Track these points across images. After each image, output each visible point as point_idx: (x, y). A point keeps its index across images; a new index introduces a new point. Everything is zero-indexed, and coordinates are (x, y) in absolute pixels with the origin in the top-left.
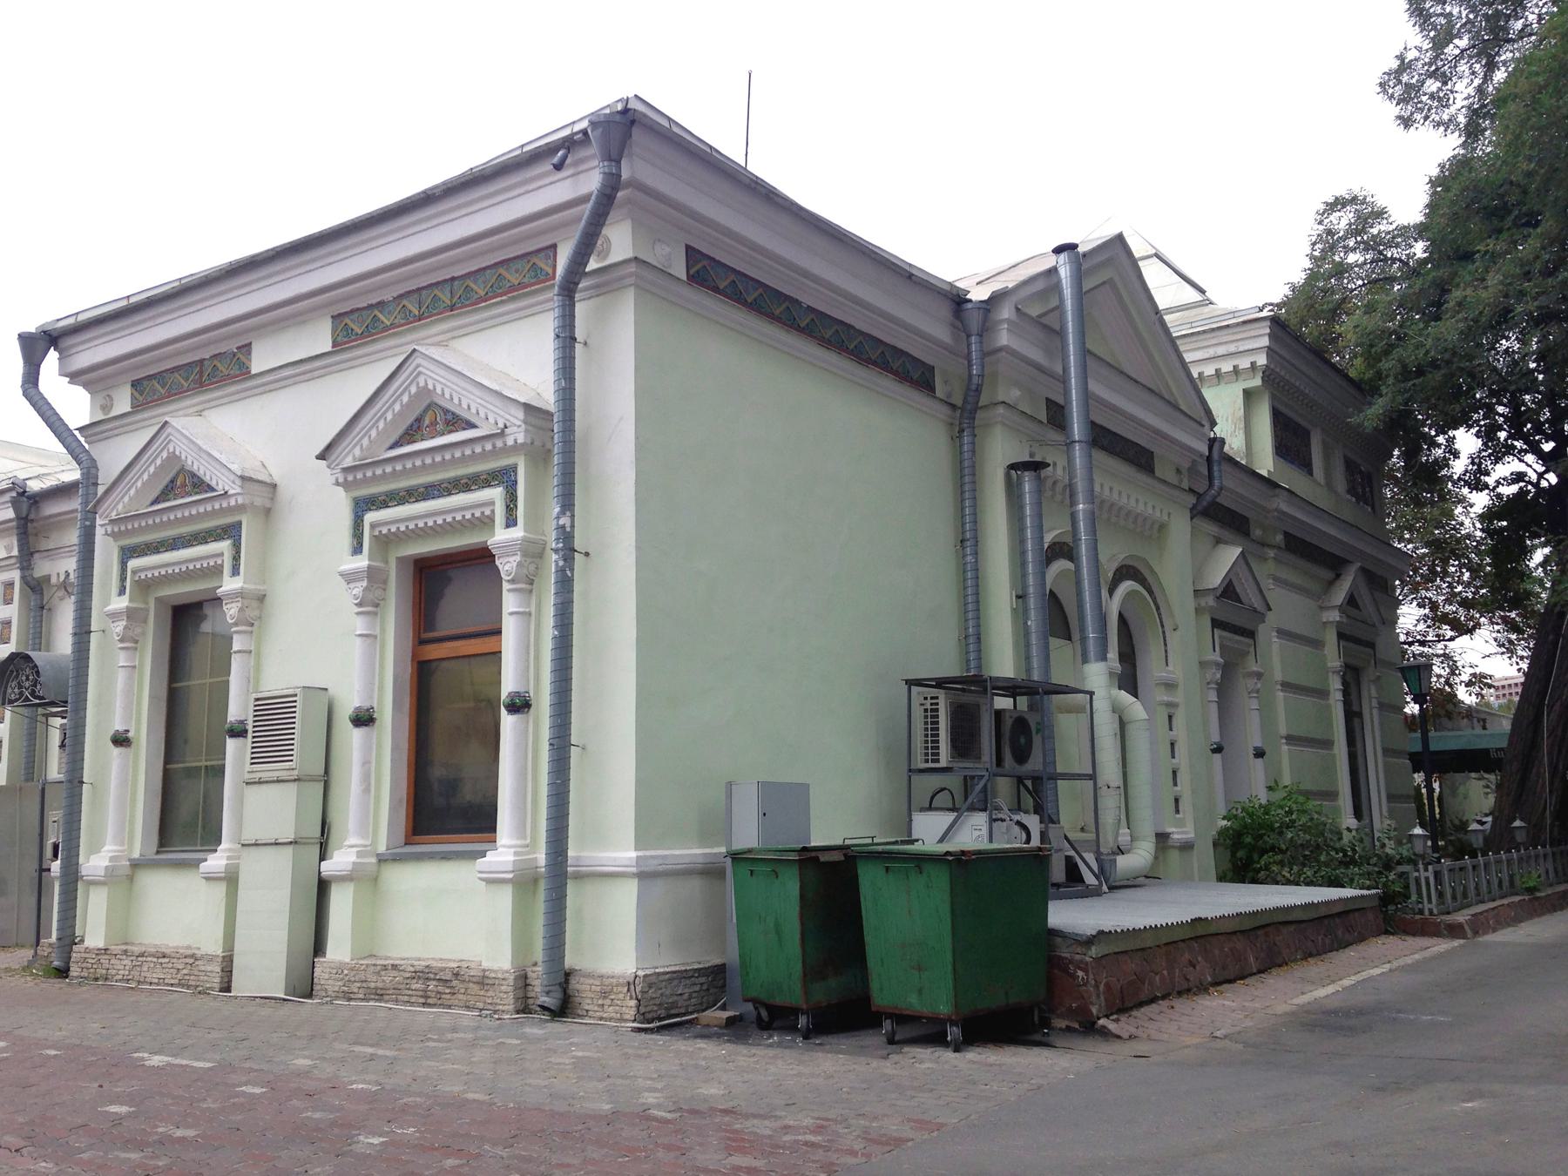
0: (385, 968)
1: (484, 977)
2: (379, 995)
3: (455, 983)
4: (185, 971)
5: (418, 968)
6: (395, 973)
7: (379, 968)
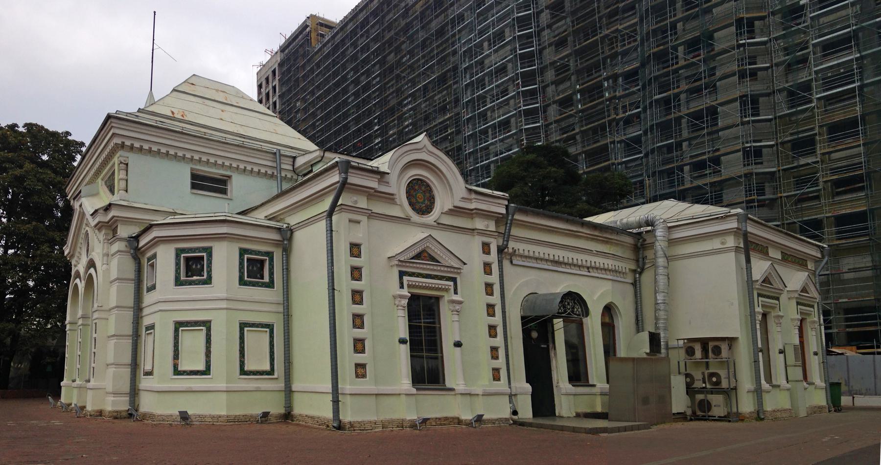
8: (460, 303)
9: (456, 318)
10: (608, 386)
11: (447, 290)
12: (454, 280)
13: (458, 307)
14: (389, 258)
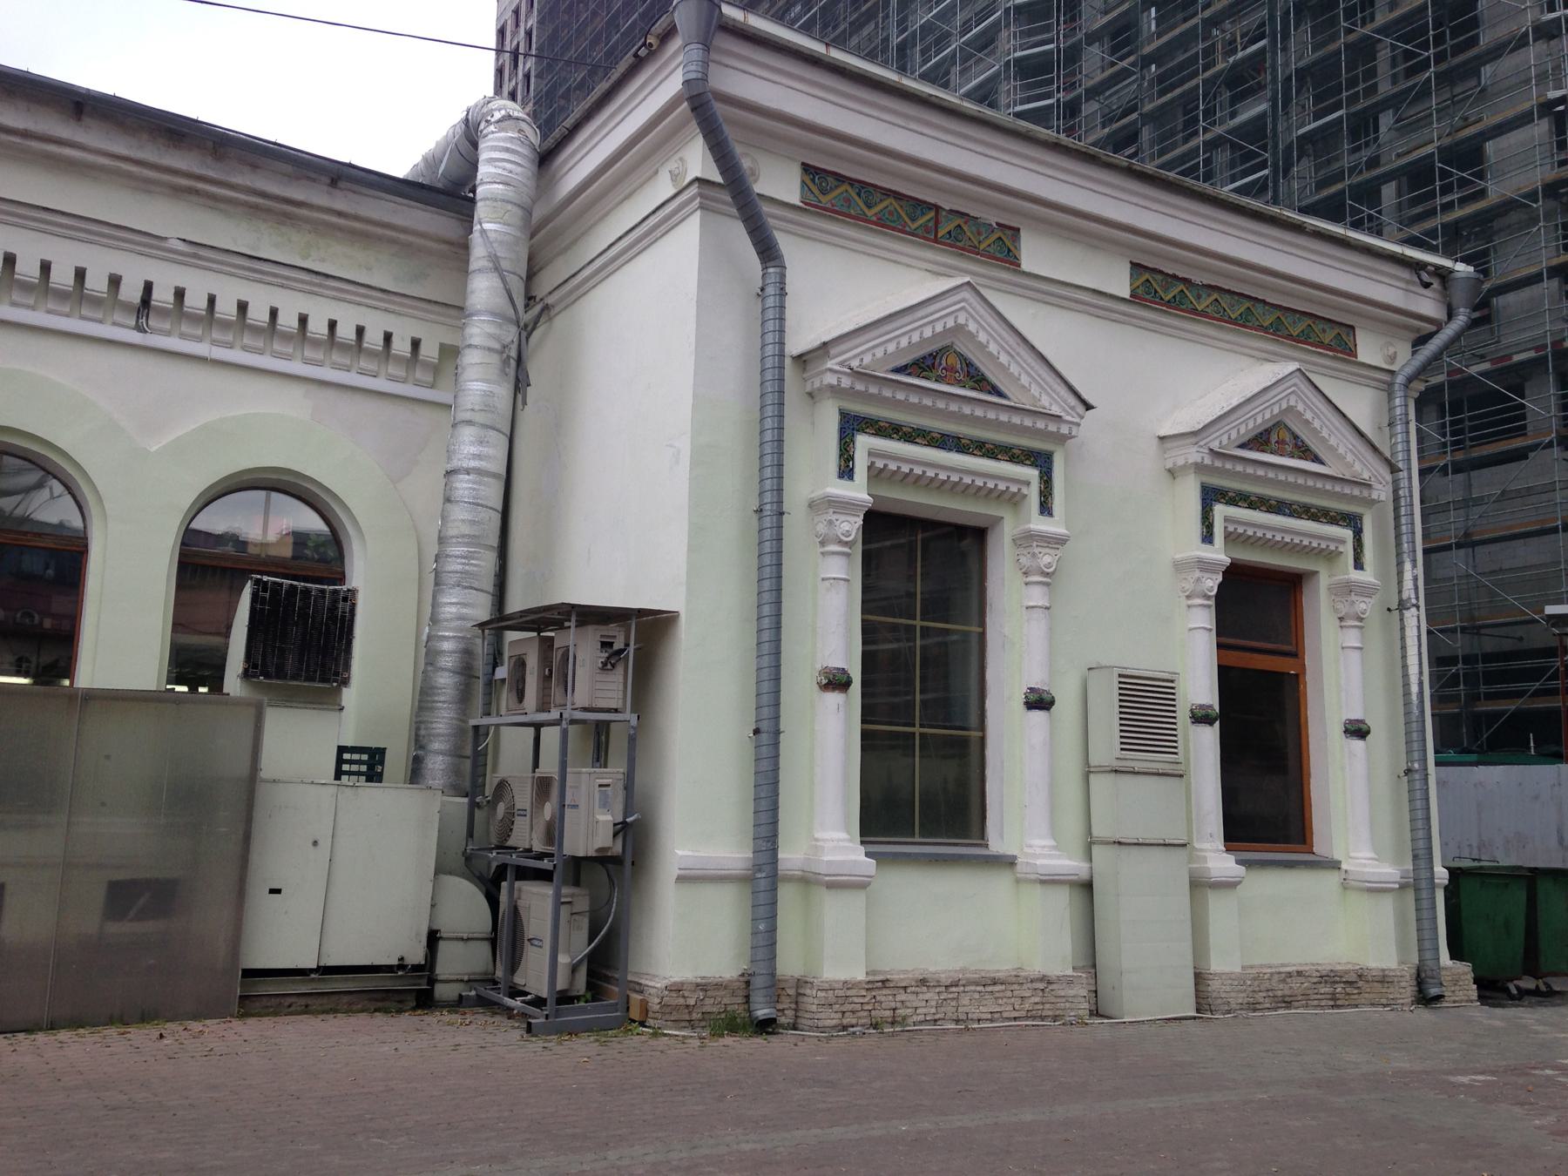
0: (1289, 975)
1: (1384, 976)
2: (1288, 1004)
3: (1360, 984)
4: (1037, 1000)
5: (1324, 973)
6: (1302, 979)
7: (1283, 975)
8: (1058, 541)
9: (1037, 596)
10: (1085, 865)
11: (1330, 556)
12: (1042, 461)
13: (1047, 559)
14: (1162, 438)
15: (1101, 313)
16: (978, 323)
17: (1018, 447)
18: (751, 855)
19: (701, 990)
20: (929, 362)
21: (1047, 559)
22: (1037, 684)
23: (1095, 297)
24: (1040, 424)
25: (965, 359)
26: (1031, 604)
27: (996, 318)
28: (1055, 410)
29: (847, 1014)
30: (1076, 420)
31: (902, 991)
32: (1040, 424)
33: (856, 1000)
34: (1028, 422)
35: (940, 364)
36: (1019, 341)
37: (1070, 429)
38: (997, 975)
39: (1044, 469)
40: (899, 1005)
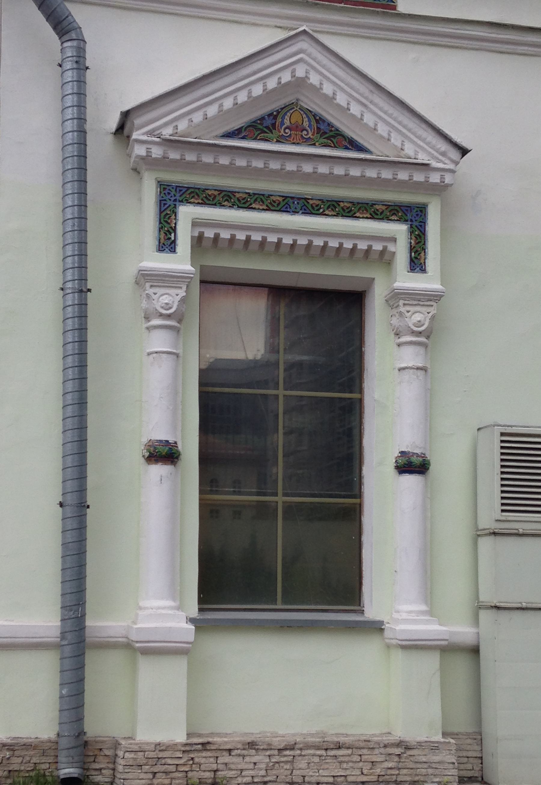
4: (390, 765)
15: (505, 47)
16: (321, 74)
17: (382, 202)
18: (59, 624)
19: (8, 749)
20: (268, 122)
21: (417, 317)
22: (407, 447)
23: (494, 30)
24: (403, 175)
25: (315, 116)
26: (403, 365)
27: (341, 65)
28: (422, 158)
29: (158, 775)
30: (451, 166)
31: (226, 754)
32: (403, 175)
33: (169, 761)
34: (387, 174)
35: (282, 123)
36: (372, 88)
37: (442, 177)
38: (342, 739)
39: (415, 223)
40: (220, 767)
